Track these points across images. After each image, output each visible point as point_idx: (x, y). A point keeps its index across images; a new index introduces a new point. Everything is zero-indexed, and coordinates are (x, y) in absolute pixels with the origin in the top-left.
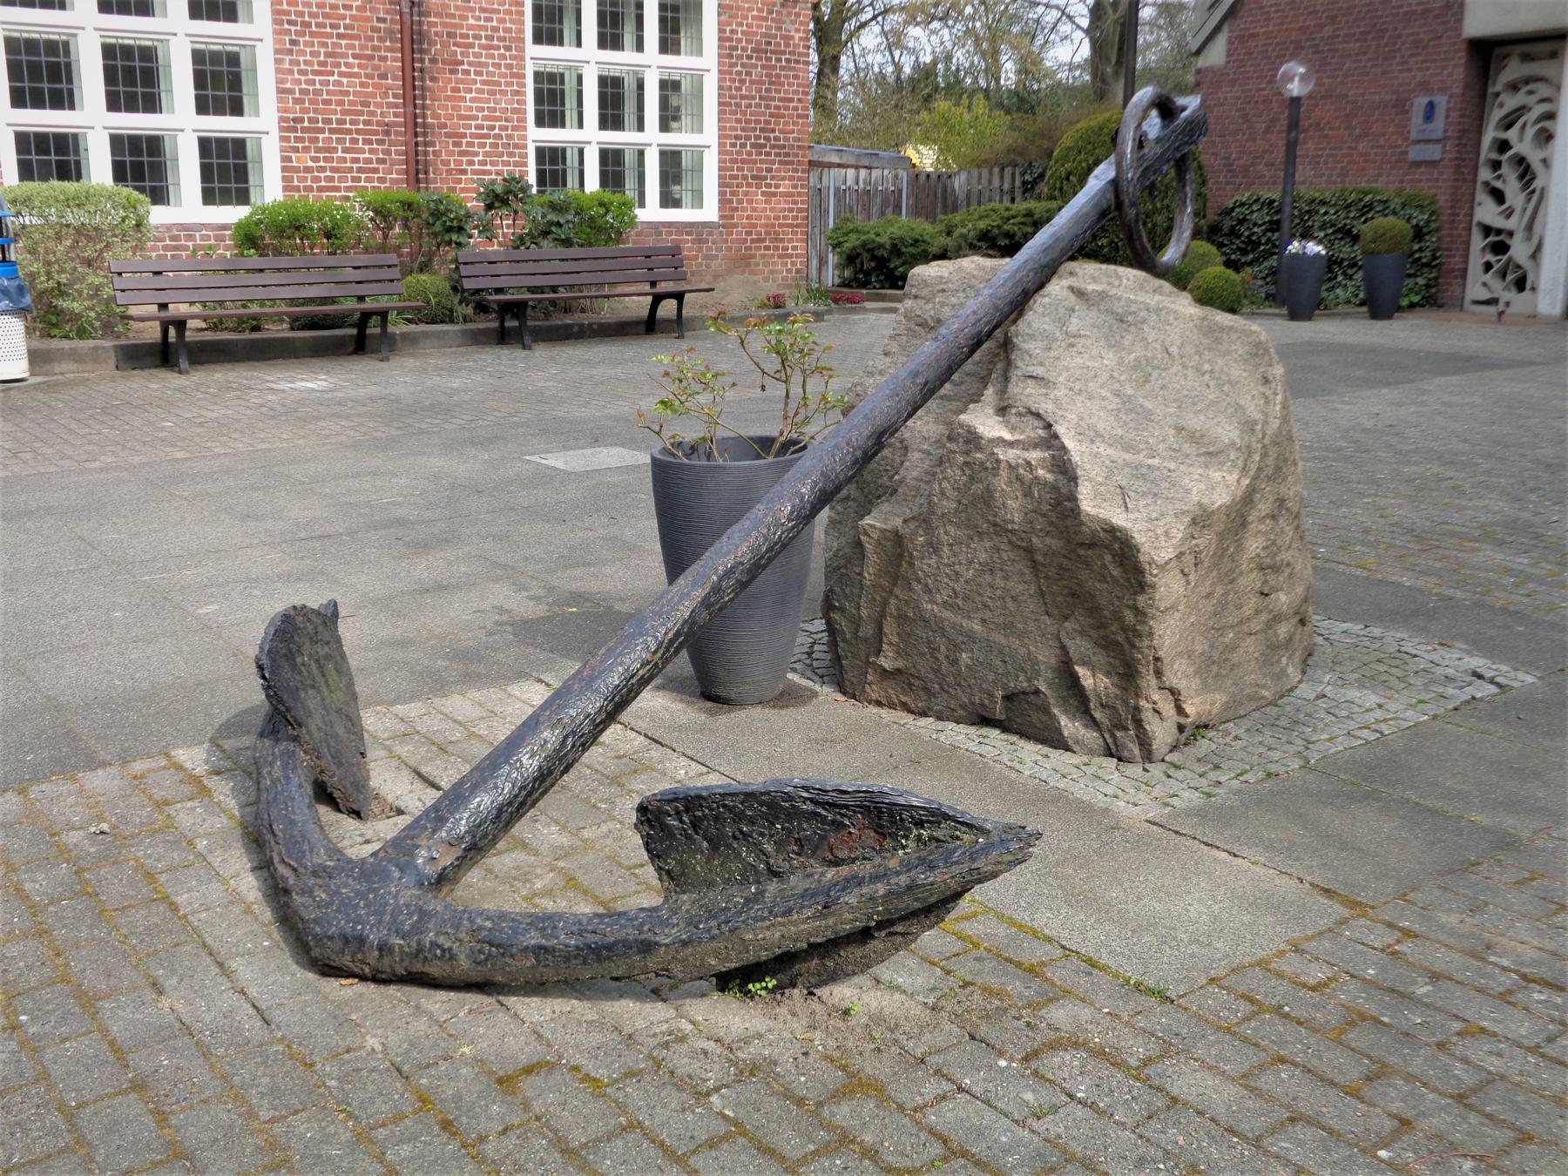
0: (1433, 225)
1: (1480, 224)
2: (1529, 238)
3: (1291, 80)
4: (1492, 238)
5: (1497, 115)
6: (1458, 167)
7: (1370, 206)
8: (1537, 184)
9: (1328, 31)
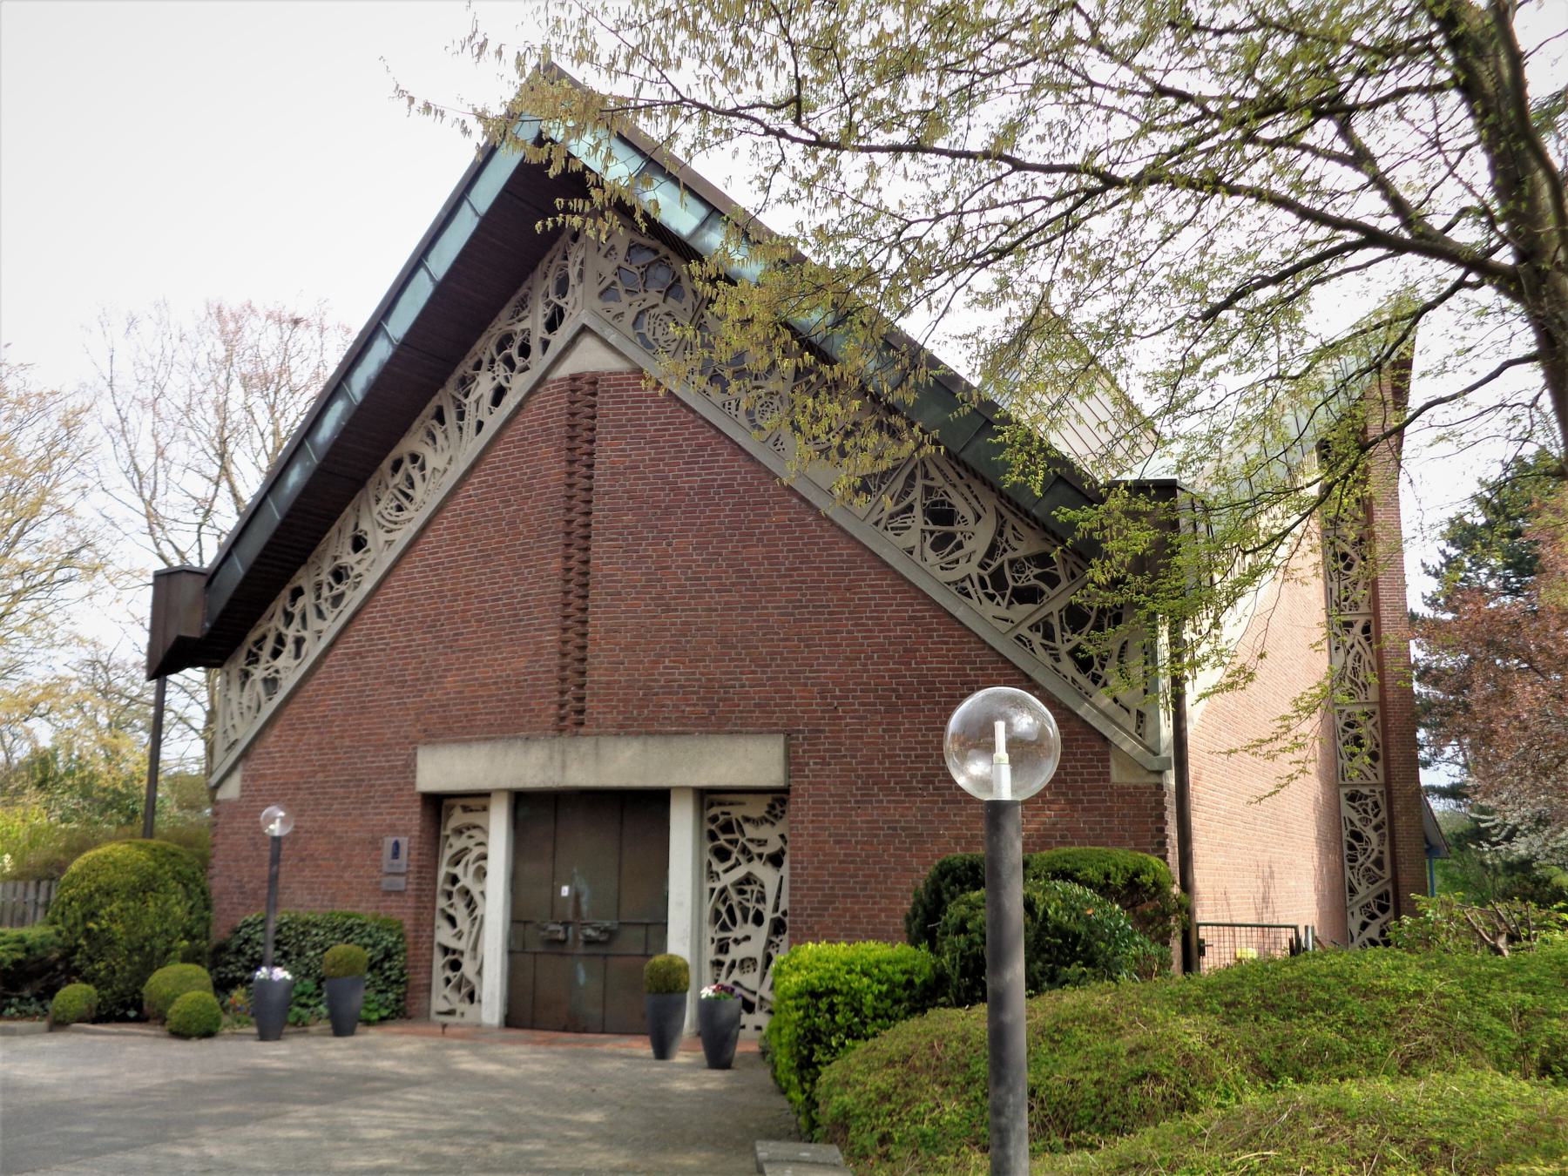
0: (400, 946)
1: (440, 945)
2: (475, 958)
3: (273, 821)
4: (450, 957)
5: (448, 853)
6: (419, 897)
7: (351, 929)
8: (478, 912)
9: (320, 777)
